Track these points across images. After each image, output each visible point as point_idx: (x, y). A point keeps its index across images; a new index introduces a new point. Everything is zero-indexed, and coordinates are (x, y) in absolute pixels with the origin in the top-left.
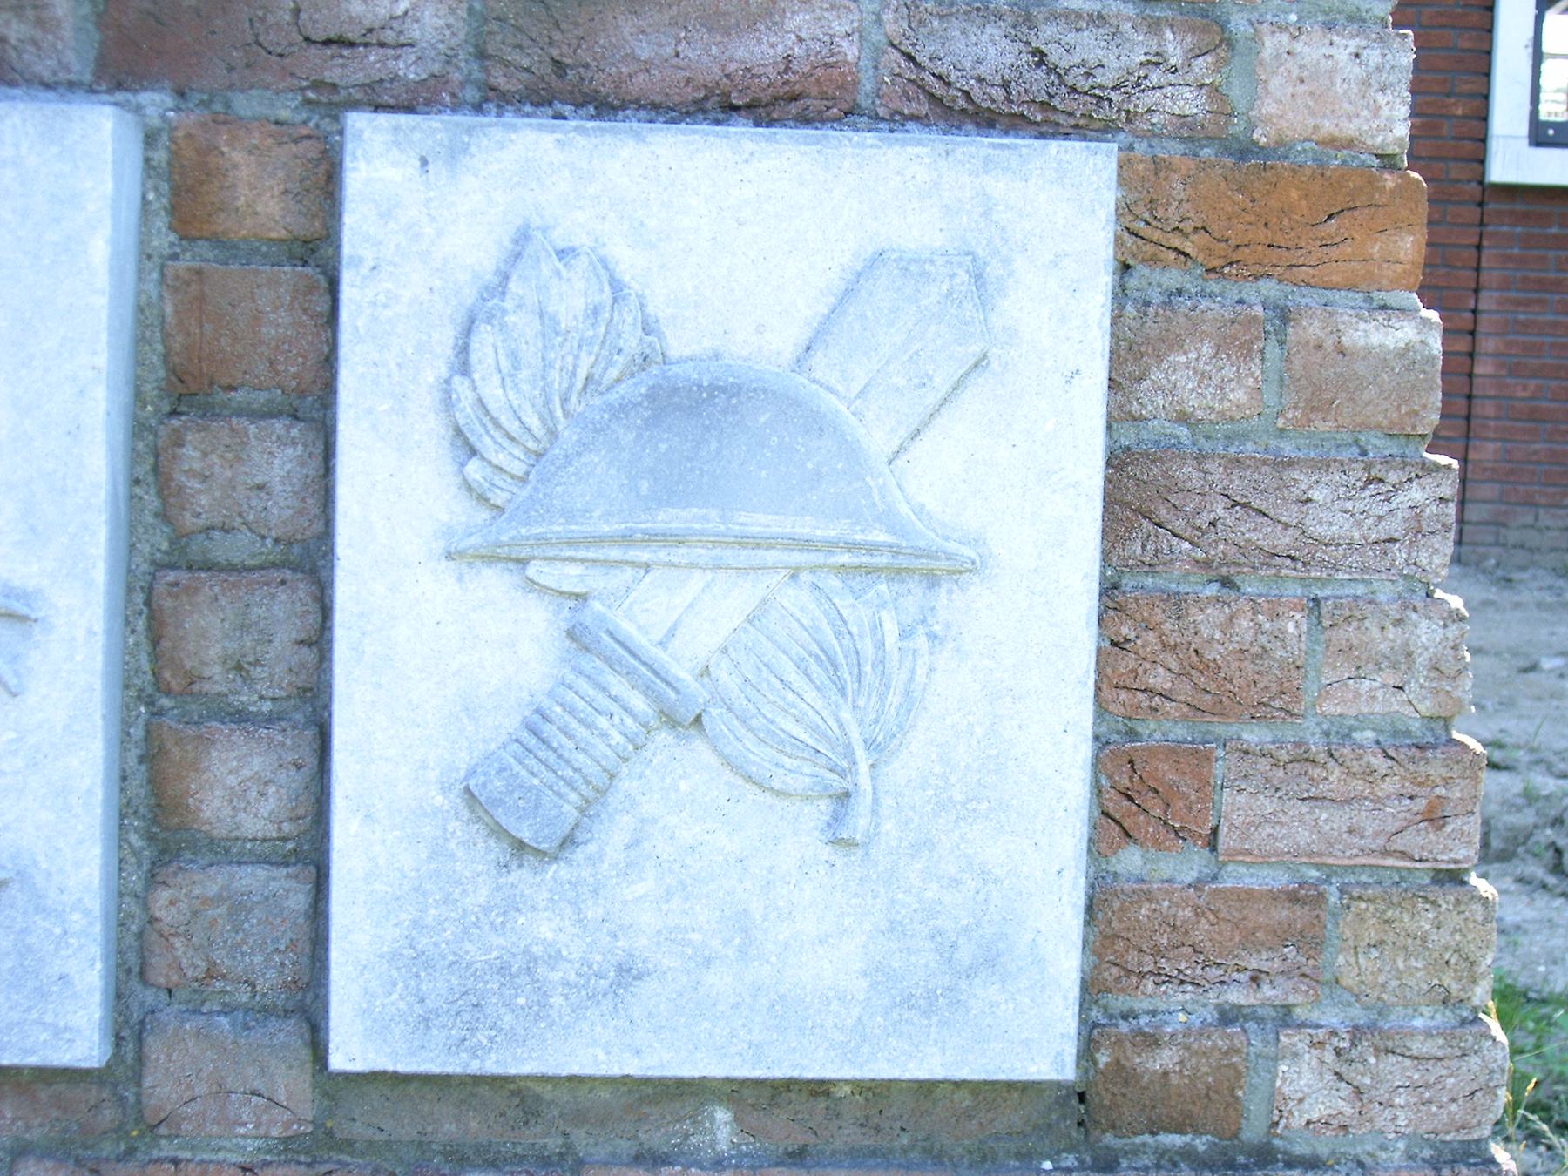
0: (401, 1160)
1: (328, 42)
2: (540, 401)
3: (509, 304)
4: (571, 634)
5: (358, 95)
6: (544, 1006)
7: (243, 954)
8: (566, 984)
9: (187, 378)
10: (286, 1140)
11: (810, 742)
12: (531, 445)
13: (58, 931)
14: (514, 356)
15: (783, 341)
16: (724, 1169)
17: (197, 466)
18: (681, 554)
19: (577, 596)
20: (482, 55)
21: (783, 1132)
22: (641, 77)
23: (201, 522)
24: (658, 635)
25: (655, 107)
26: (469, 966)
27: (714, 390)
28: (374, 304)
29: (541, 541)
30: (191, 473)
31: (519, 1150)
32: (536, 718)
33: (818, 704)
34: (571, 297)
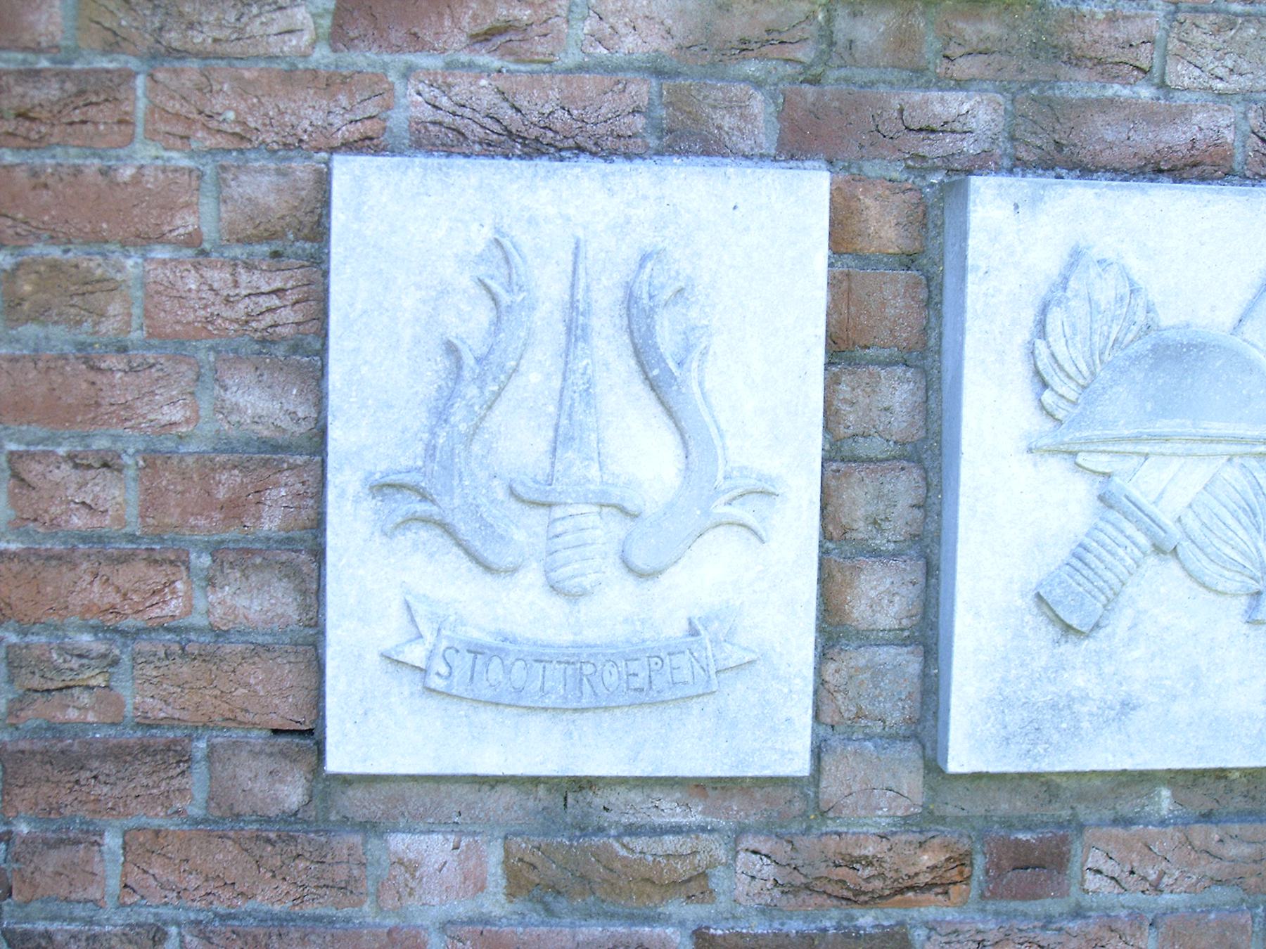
0: (973, 828)
1: (921, 130)
2: (1088, 354)
3: (1069, 294)
4: (1101, 498)
5: (939, 163)
6: (1077, 728)
7: (879, 702)
8: (1091, 714)
9: (839, 341)
10: (905, 818)
11: (1241, 561)
12: (1081, 381)
13: (786, 690)
14: (1073, 326)
15: (1226, 317)
16: (1167, 826)
17: (848, 396)
18: (1167, 448)
19: (1104, 474)
20: (1012, 138)
21: (1200, 801)
22: (1108, 151)
23: (850, 431)
24: (1152, 498)
25: (1115, 170)
26: (1034, 704)
27: (1190, 346)
28: (986, 295)
29: (1089, 441)
30: (845, 401)
31: (1045, 819)
32: (1080, 550)
33: (1246, 538)
34: (1106, 291)
